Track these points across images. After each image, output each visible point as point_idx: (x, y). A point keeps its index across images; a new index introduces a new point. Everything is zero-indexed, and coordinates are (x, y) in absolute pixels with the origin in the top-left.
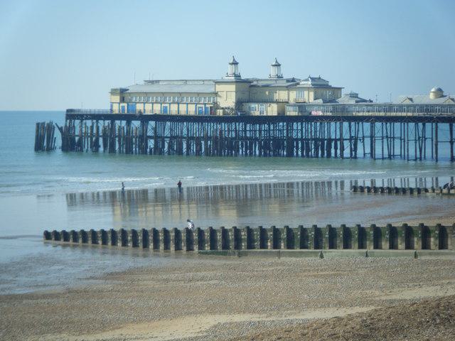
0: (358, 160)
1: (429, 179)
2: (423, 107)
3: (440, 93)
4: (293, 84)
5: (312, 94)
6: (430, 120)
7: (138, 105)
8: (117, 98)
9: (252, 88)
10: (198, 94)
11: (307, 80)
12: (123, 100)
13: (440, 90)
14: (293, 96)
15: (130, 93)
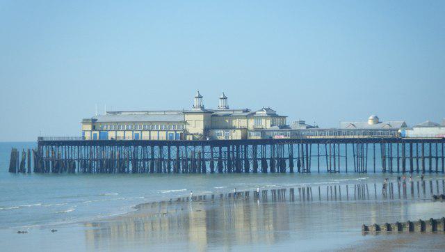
0: (341, 173)
1: (343, 187)
2: (366, 131)
3: (376, 120)
4: (249, 114)
5: (269, 122)
6: (298, 141)
7: (110, 132)
8: (89, 127)
9: (213, 118)
10: (168, 123)
11: (262, 110)
12: (94, 128)
13: (376, 118)
14: (251, 123)
15: (101, 123)
